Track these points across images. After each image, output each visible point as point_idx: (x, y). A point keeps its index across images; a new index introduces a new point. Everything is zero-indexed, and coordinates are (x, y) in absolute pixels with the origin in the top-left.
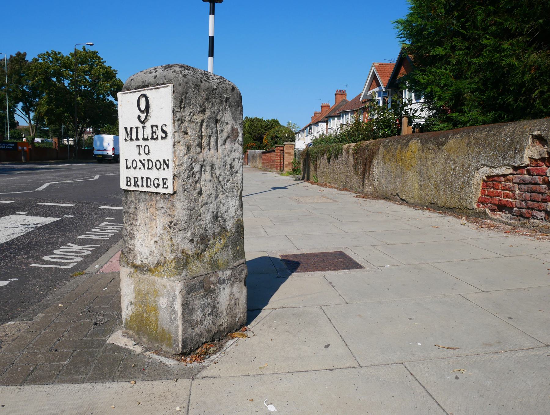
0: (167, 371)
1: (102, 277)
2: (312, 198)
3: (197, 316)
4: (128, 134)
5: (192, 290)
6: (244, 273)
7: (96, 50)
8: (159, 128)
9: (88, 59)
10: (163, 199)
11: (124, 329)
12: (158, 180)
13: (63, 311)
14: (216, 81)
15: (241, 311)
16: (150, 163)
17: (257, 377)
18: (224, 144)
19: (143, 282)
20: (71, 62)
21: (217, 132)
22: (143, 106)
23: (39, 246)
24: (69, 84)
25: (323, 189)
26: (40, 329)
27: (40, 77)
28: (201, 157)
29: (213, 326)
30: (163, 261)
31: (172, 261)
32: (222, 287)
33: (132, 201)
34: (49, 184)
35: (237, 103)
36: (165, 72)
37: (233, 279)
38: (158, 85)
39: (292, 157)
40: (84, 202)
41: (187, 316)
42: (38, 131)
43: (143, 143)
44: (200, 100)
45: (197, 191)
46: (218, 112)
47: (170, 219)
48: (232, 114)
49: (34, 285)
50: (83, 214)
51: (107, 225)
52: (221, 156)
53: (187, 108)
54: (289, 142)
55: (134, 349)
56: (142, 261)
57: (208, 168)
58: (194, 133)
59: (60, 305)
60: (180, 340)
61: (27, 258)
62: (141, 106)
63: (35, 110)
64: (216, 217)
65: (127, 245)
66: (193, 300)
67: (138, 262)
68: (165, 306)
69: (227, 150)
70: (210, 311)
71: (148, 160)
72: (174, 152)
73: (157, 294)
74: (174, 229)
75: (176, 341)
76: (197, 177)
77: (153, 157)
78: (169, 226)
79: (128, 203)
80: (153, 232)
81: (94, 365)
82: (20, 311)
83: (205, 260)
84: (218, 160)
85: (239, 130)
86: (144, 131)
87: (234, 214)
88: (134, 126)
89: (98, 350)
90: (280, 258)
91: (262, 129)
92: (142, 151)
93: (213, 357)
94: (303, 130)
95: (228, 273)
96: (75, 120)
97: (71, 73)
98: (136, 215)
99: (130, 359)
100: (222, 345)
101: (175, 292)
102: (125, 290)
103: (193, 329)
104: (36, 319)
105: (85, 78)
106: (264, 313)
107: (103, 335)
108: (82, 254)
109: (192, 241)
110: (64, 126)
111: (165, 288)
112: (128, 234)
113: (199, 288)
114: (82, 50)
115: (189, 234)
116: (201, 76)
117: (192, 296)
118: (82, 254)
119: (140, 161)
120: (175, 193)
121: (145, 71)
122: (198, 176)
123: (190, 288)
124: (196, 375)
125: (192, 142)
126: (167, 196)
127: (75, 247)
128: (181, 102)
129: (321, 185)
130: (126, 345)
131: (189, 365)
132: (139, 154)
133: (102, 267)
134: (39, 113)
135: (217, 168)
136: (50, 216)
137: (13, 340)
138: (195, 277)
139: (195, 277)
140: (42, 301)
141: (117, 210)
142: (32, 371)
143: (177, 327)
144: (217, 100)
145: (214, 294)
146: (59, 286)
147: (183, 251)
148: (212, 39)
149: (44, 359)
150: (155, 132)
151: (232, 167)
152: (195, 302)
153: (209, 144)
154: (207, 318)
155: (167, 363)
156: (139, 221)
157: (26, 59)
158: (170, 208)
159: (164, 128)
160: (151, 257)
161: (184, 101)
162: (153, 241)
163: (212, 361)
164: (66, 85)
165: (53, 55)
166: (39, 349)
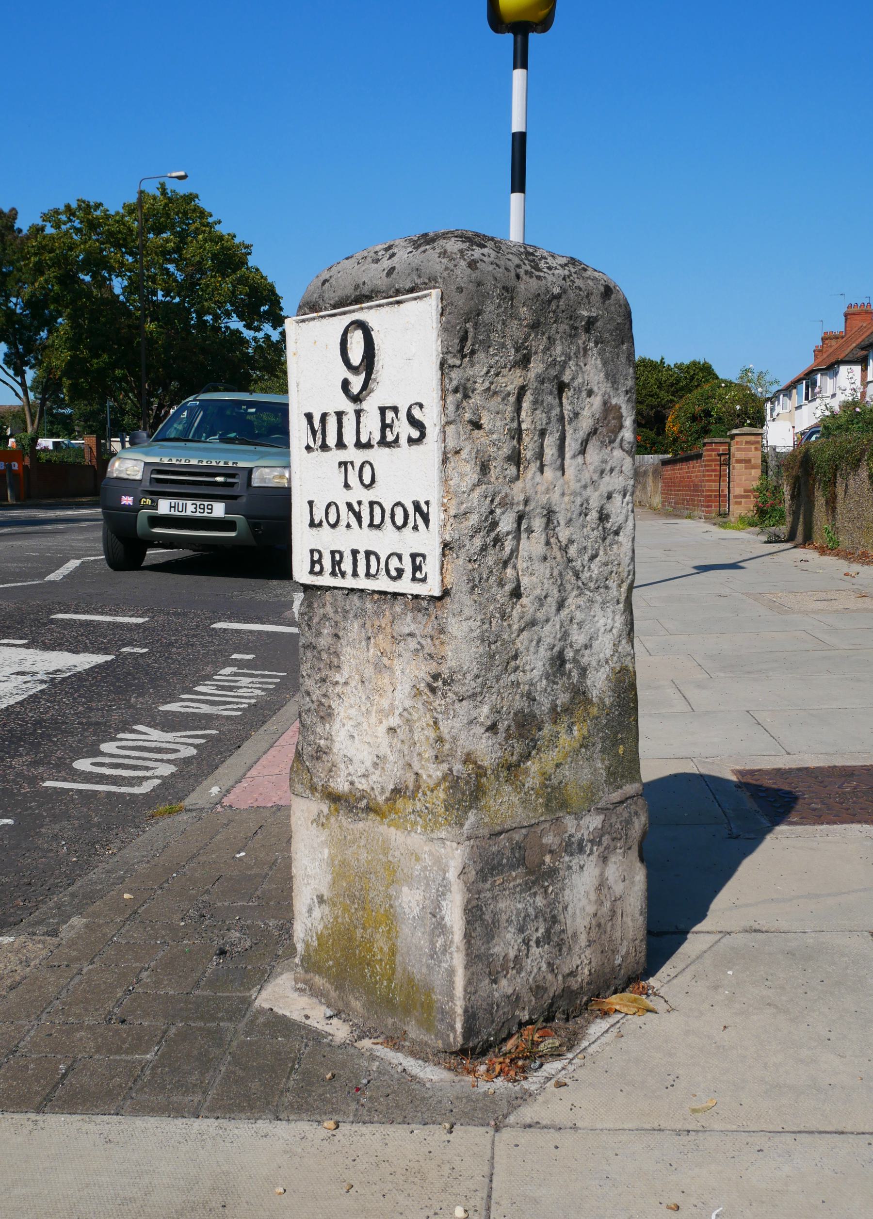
0: (423, 1099)
1: (230, 821)
2: (823, 595)
3: (507, 943)
4: (314, 432)
5: (493, 868)
6: (639, 823)
7: (194, 191)
8: (403, 414)
9: (173, 216)
10: (412, 610)
11: (300, 969)
12: (400, 557)
13: (136, 912)
14: (560, 272)
15: (630, 934)
16: (377, 510)
17: (684, 1139)
18: (583, 452)
19: (354, 841)
20: (130, 230)
21: (561, 418)
22: (356, 355)
23: (63, 732)
24: (124, 289)
25: (856, 567)
26: (78, 959)
27: (51, 273)
28: (517, 493)
29: (550, 977)
30: (411, 785)
31: (438, 784)
32: (575, 862)
33: (325, 617)
34: (79, 561)
35: (624, 332)
36: (417, 258)
37: (606, 840)
38: (398, 292)
39: (756, 473)
40: (172, 610)
41: (477, 943)
42: (46, 418)
43: (357, 456)
44: (515, 330)
45: (508, 588)
46: (565, 362)
47: (433, 667)
48: (605, 363)
49: (55, 838)
50: (171, 644)
51: (236, 674)
52: (575, 486)
53: (481, 355)
54: (746, 429)
55: (328, 1029)
56: (352, 783)
57: (538, 523)
59: (127, 896)
60: (459, 1011)
61: (35, 764)
63: (39, 363)
64: (559, 661)
65: (312, 737)
66: (495, 898)
67: (341, 785)
68: (417, 911)
69: (591, 468)
70: (542, 930)
71: (372, 504)
72: (445, 480)
73: (393, 875)
74: (444, 696)
75: (447, 1015)
76: (508, 550)
77: (385, 494)
78: (429, 685)
79: (316, 620)
80: (385, 703)
81: (223, 1069)
82: (22, 908)
84: (566, 499)
85: (624, 411)
86: (358, 423)
87: (608, 652)
88: (331, 410)
89: (231, 1026)
90: (734, 778)
91: (662, 394)
92: (353, 480)
93: (552, 1067)
94: (787, 391)
95: (594, 822)
96: (140, 387)
97: (131, 259)
98: (337, 654)
99: (319, 1058)
100: (575, 1034)
102: (306, 861)
103: (495, 981)
104: (66, 932)
105: (167, 269)
106: (695, 943)
107: (242, 984)
108: (172, 756)
109: (492, 728)
110: (110, 403)
111: (418, 859)
112: (314, 706)
113: (512, 864)
114: (158, 193)
115: (486, 710)
116: (517, 261)
117: (493, 885)
118: (172, 756)
119: (349, 506)
120: (446, 593)
121: (359, 255)
122: (509, 544)
123: (487, 863)
124: (505, 1116)
125: (492, 449)
126: (424, 604)
127: (156, 736)
128: (463, 339)
129: (849, 556)
130: (307, 1017)
131: (484, 1086)
132: (347, 486)
133: (228, 791)
134: (49, 370)
135: (562, 523)
136: (86, 650)
137: (12, 988)
138: (500, 833)
139: (500, 833)
140: (79, 883)
141: (260, 633)
142: (64, 1076)
143: (451, 972)
144: (564, 327)
145: (553, 884)
146: (117, 843)
147: (468, 759)
148: (520, 140)
150: (391, 426)
151: (603, 517)
152: (502, 905)
153: (540, 455)
154: (535, 950)
155: (421, 1075)
156: (346, 671)
157: (17, 226)
158: (432, 638)
159: (416, 413)
160: (378, 773)
161: (471, 335)
162: (382, 730)
163: (549, 1079)
164: (117, 290)
165: (80, 214)
166: (78, 1016)
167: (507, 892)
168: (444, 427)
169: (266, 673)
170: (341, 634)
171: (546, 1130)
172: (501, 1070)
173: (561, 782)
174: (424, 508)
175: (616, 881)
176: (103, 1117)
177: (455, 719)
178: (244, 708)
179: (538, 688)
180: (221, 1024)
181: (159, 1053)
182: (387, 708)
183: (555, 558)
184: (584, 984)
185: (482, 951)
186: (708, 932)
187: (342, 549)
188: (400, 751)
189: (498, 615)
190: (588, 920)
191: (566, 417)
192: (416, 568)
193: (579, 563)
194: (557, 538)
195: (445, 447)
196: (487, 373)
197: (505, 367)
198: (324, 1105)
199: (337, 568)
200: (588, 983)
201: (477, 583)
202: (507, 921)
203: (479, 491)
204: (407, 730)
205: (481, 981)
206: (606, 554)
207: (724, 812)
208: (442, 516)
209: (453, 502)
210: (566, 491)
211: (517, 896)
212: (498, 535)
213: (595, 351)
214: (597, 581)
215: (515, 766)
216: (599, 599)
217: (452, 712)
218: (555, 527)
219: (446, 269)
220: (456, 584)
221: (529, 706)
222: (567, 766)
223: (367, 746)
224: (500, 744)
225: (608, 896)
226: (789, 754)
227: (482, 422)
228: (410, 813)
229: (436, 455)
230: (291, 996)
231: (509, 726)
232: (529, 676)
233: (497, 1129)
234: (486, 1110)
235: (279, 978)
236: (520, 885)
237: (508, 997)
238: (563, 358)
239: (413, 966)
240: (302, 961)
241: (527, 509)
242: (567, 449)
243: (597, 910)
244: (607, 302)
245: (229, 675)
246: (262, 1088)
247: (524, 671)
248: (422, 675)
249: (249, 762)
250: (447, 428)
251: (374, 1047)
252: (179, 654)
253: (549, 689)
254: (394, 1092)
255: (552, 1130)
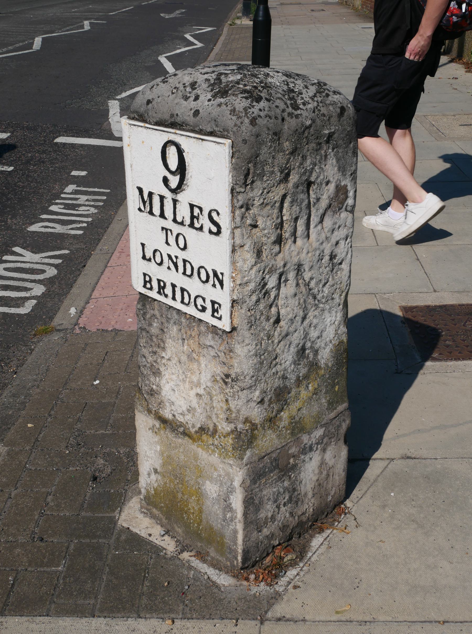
0: (220, 600)
3: (268, 509)
4: (144, 202)
5: (260, 476)
8: (206, 213)
12: (204, 300)
15: (337, 483)
16: (188, 266)
18: (321, 221)
22: (173, 163)
29: (291, 519)
30: (211, 429)
32: (307, 458)
37: (325, 440)
43: (176, 229)
46: (313, 169)
47: (225, 370)
48: (338, 160)
52: (315, 245)
53: (258, 183)
55: (162, 544)
56: (174, 416)
57: (291, 275)
58: (268, 223)
59: (29, 425)
60: (240, 551)
62: (168, 162)
64: (302, 351)
65: (147, 382)
66: (261, 491)
67: (167, 414)
68: (215, 495)
69: (326, 230)
70: (287, 498)
72: (233, 263)
74: (232, 387)
75: (234, 552)
76: (272, 297)
77: (196, 256)
79: (148, 316)
80: (195, 379)
83: (282, 424)
84: (310, 255)
87: (332, 336)
90: (400, 313)
92: (172, 240)
93: (292, 573)
95: (319, 433)
98: (164, 342)
101: (232, 482)
103: (260, 531)
108: (41, 277)
111: (216, 470)
112: (148, 365)
115: (257, 393)
117: (260, 485)
118: (41, 277)
119: (170, 257)
120: (234, 329)
124: (266, 612)
125: (264, 239)
127: (29, 257)
128: (246, 172)
131: (255, 589)
132: (167, 243)
135: (307, 269)
138: (264, 457)
142: (13, 585)
143: (235, 532)
147: (247, 420)
149: (25, 559)
151: (332, 257)
152: (265, 493)
153: (294, 234)
155: (218, 581)
158: (225, 354)
159: (214, 215)
161: (251, 171)
167: (268, 485)
168: (233, 229)
169: (96, 190)
170: (165, 330)
171: (288, 622)
172: (263, 578)
173: (301, 418)
174: (220, 276)
175: (330, 459)
176: (40, 618)
177: (239, 400)
178: (84, 227)
179: (289, 371)
180: (100, 541)
181: (66, 565)
182: (196, 381)
183: (301, 293)
184: (310, 516)
185: (253, 519)
186: (381, 459)
187: (165, 281)
188: (204, 408)
189: (266, 338)
190: (313, 484)
191: (312, 203)
192: (214, 310)
193: (316, 290)
194: (303, 279)
195: (234, 243)
196: (262, 193)
197: (274, 186)
198: (165, 606)
199: (162, 291)
200: (312, 515)
201: (253, 323)
202: (268, 499)
203: (255, 268)
204: (209, 398)
205: (252, 533)
206: (333, 279)
207: (394, 348)
208: (232, 285)
209: (239, 276)
210: (310, 250)
211: (274, 485)
212: (266, 290)
213: (332, 154)
214: (327, 297)
215: (274, 418)
216: (328, 307)
217: (237, 397)
218: (302, 273)
219: (236, 125)
220: (241, 325)
221: (283, 383)
222: (304, 408)
223: (183, 399)
224: (265, 409)
225: (325, 468)
226: (435, 291)
227: (258, 223)
228: (211, 445)
229: (228, 248)
230: (139, 517)
231: (271, 397)
232: (283, 366)
233: (262, 623)
234: (256, 608)
235: (131, 502)
236: (275, 479)
237: (267, 536)
238: (311, 167)
239: (213, 522)
240: (145, 498)
241: (285, 269)
242: (311, 223)
243: (319, 477)
244: (342, 119)
245: (71, 193)
246: (128, 594)
247: (281, 364)
248: (218, 372)
249: (93, 283)
250: (235, 231)
251: (190, 558)
252: (35, 171)
253: (295, 370)
254: (204, 595)
255: (292, 623)
